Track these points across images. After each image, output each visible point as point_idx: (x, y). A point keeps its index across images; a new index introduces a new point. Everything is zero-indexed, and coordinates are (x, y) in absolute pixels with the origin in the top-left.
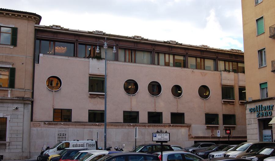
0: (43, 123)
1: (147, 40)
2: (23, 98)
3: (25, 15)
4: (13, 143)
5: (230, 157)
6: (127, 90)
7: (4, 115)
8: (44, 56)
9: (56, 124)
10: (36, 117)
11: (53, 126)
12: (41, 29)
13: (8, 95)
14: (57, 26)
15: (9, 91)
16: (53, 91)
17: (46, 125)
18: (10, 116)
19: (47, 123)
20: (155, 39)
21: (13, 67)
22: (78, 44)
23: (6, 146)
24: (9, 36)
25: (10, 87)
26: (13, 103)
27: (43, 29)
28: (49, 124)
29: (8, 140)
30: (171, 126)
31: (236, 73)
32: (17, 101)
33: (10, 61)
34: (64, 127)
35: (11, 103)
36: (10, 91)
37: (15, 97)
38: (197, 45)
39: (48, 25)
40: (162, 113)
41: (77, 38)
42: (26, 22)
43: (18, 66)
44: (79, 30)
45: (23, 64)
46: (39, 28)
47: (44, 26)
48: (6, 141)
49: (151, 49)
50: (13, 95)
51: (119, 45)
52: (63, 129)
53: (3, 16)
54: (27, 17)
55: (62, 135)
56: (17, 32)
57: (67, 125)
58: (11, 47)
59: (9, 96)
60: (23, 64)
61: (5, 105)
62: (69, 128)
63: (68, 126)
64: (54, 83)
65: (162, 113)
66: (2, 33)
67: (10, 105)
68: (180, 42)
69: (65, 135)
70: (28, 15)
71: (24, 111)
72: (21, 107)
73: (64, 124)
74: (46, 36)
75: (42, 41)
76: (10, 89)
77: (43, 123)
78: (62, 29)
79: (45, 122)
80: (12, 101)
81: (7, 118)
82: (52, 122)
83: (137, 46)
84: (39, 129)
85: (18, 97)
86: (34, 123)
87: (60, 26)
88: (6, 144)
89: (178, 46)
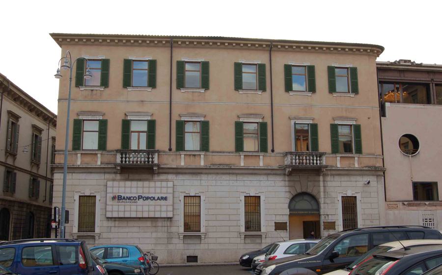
0: (401, 203)
1: (420, 65)
2: (375, 167)
3: (291, 44)
4: (210, 235)
5: (276, 258)
6: (403, 145)
7: (92, 192)
8: (392, 105)
9: (419, 205)
10: (391, 195)
11: (415, 208)
12: (384, 66)
13: (354, 164)
14: (405, 61)
15: (78, 155)
16: (409, 156)
17: (405, 206)
18: (360, 194)
19: (406, 203)
20: (387, 61)
21: (153, 119)
22: (434, 84)
23: (95, 240)
24: (198, 75)
25: (262, 151)
26: (362, 175)
27: (387, 66)
28: (409, 205)
29: (203, 230)
30: (426, 204)
31: (422, 103)
32: (367, 173)
33: (352, 115)
34: (429, 208)
35: (360, 175)
36: (243, 156)
37: (366, 167)
38: (391, 61)
39: (393, 61)
40: (436, 183)
41: (432, 76)
42: (366, 58)
43: (363, 123)
44: (435, 64)
45: (369, 118)
46: (382, 66)
47: (389, 62)
48: (94, 232)
49: (428, 79)
50: (361, 164)
51: (435, 80)
52: (429, 212)
53: (114, 44)
54: (84, 40)
55: (428, 220)
56: (285, 71)
57: (434, 206)
58: (148, 90)
59: (356, 165)
60: (369, 118)
61: (353, 178)
62: (436, 210)
63: (434, 208)
64: (410, 144)
65: (436, 183)
66: (187, 71)
67: (359, 178)
68: (418, 62)
69: (432, 220)
70: (370, 48)
71: (376, 184)
72: (372, 179)
73: (430, 205)
74: (390, 76)
75: (384, 85)
76: (262, 154)
77: (401, 203)
78: (413, 64)
79: (403, 202)
80: (361, 172)
81: (260, 197)
82: (412, 201)
83: (404, 77)
84: (396, 212)
85: (369, 167)
86: (389, 203)
87: (409, 61)
88: (200, 236)
89: (416, 68)
